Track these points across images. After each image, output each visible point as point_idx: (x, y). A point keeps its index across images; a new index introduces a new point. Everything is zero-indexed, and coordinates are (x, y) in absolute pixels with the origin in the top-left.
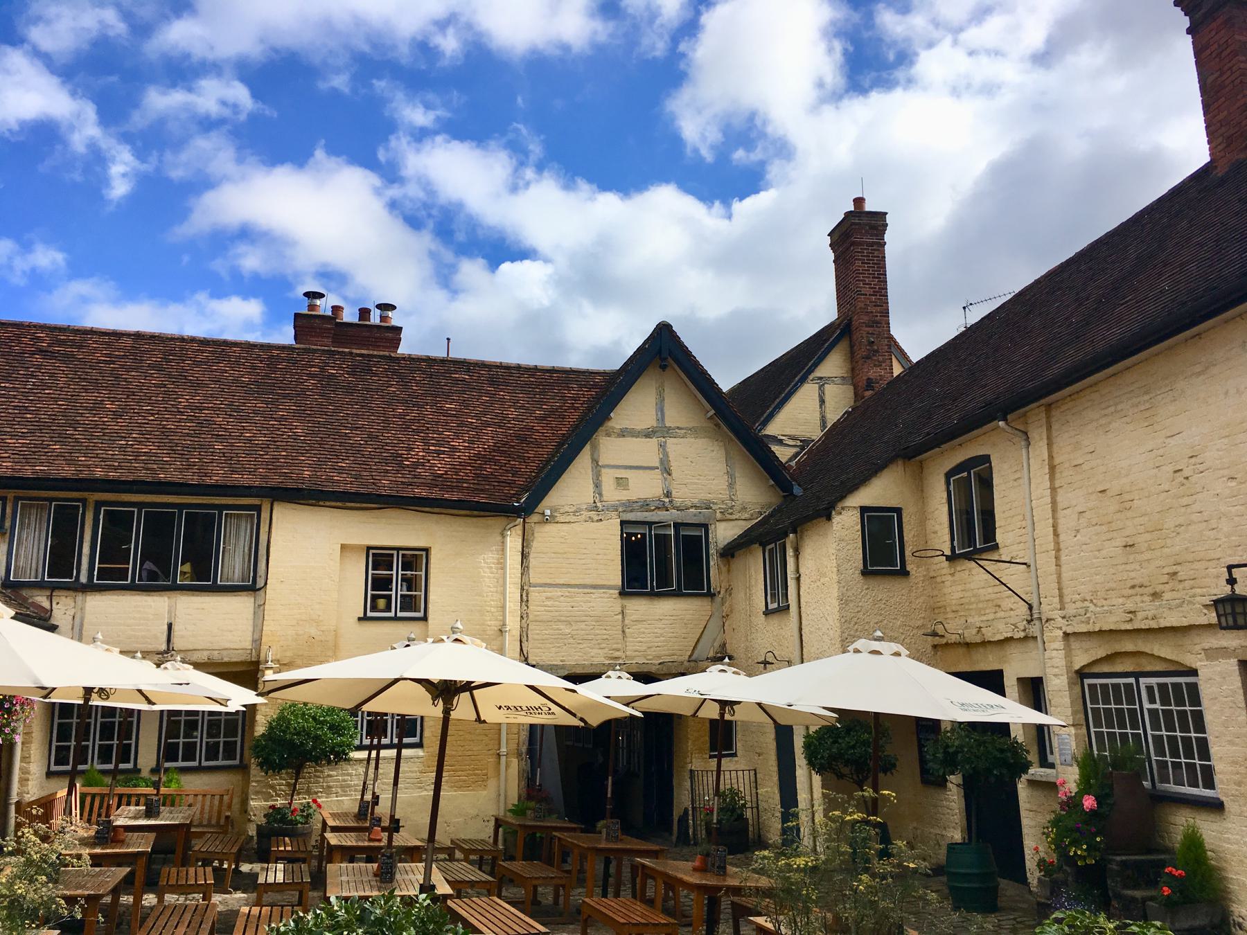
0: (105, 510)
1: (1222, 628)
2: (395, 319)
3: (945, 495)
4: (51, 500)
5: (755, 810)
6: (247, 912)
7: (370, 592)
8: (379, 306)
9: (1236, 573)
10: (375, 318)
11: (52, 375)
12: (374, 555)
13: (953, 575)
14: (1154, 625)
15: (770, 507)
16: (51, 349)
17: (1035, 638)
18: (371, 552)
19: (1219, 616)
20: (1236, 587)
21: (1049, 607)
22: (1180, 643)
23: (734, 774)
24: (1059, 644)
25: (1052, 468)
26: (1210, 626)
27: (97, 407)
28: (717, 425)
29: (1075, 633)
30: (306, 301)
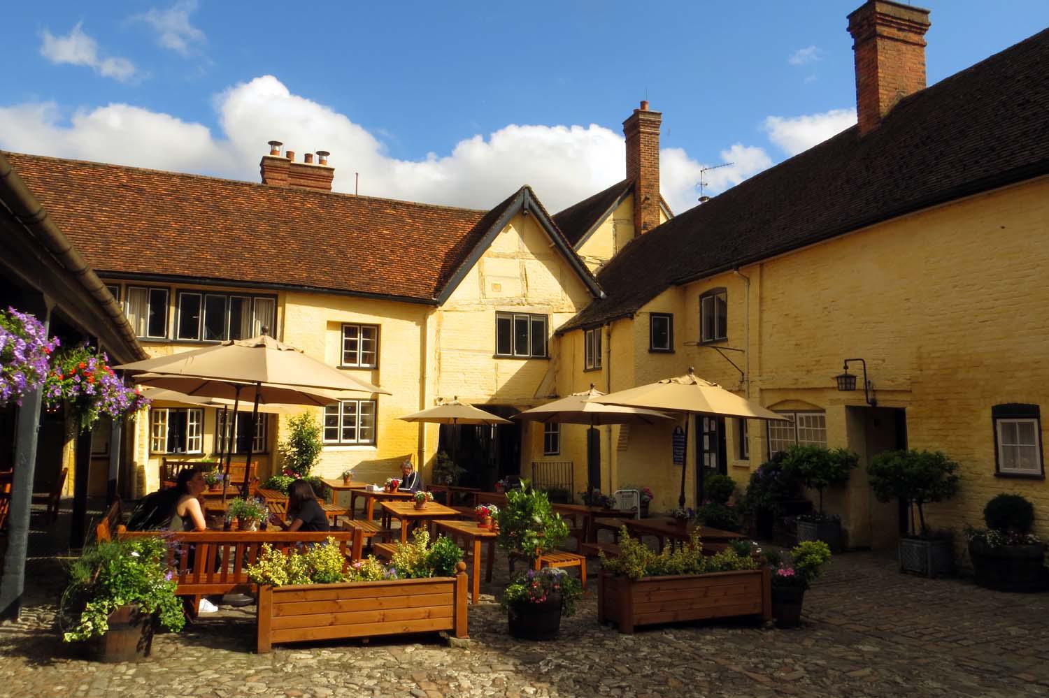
0: (182, 295)
1: (839, 390)
2: (330, 162)
3: (698, 308)
4: (149, 287)
5: (571, 486)
6: (731, 419)
7: (344, 351)
8: (319, 153)
9: (848, 363)
10: (315, 162)
11: (134, 203)
12: (363, 329)
13: (700, 354)
14: (806, 386)
15: (585, 304)
16: (129, 184)
17: (744, 391)
18: (344, 326)
19: (838, 384)
20: (848, 370)
21: (753, 375)
22: (505, 661)
23: (549, 465)
24: (757, 394)
25: (761, 299)
26: (833, 388)
27: (166, 226)
28: (555, 252)
29: (766, 389)
30: (269, 147)
